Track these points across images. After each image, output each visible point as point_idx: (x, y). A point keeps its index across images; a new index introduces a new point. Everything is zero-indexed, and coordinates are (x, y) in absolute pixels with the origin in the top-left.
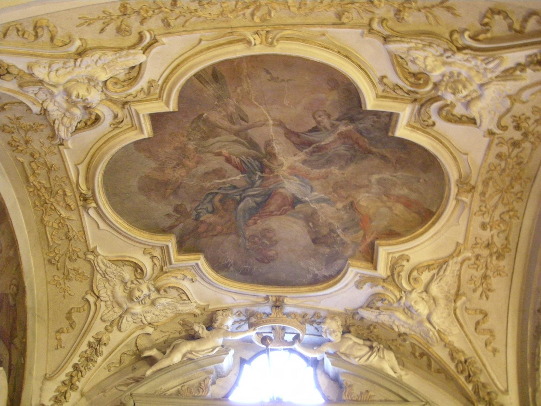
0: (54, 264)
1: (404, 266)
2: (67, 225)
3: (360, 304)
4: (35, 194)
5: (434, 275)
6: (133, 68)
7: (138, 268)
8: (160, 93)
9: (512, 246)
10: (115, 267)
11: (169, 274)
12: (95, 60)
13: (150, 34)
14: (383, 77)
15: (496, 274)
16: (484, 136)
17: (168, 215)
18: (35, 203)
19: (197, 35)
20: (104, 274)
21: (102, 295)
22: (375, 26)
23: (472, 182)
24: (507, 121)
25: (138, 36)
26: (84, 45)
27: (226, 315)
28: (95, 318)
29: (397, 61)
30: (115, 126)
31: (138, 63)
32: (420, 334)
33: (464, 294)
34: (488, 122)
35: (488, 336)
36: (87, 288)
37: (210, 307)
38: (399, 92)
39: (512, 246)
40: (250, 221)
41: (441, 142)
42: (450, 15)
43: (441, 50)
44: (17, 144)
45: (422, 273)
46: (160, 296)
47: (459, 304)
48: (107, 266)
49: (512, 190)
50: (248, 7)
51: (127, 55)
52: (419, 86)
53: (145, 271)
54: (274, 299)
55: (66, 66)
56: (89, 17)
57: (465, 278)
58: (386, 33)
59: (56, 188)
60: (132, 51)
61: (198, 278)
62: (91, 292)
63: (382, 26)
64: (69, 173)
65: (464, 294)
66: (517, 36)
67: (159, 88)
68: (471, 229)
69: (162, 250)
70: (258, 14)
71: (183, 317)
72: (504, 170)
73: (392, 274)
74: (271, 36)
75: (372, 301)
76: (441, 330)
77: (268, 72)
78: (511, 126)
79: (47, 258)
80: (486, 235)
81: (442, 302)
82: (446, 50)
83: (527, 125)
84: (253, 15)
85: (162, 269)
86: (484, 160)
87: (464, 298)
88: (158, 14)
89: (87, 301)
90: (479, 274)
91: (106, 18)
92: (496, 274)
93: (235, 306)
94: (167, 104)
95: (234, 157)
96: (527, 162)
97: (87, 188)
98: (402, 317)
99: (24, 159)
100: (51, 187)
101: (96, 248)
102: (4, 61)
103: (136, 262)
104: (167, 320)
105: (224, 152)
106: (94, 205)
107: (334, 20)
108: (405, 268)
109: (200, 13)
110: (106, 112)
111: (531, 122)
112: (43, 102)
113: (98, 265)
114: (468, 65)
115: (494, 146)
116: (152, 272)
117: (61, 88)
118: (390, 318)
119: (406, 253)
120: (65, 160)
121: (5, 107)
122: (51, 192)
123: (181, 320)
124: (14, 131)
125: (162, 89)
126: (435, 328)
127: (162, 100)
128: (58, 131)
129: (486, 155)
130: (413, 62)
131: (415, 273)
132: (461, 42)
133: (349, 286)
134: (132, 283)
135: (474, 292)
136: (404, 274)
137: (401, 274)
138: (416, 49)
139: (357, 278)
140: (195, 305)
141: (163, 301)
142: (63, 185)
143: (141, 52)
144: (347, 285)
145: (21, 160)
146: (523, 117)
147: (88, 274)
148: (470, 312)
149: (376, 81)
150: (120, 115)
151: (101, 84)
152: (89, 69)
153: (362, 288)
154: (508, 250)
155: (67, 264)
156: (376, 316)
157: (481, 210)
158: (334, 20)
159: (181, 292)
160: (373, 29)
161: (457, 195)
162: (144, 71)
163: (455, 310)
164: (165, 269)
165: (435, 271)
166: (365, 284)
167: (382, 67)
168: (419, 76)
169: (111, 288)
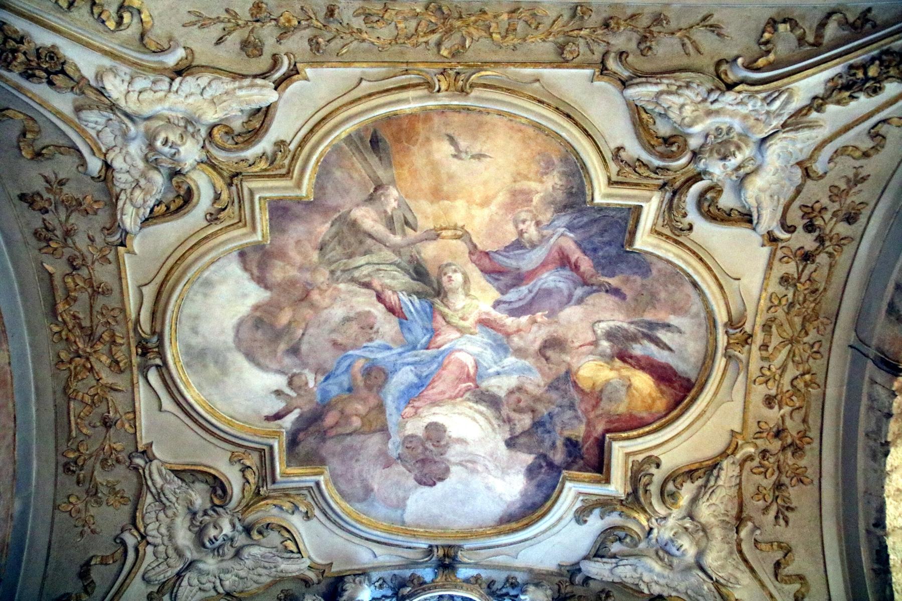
0: (74, 472)
1: (653, 475)
2: (107, 399)
3: (583, 552)
4: (62, 339)
5: (700, 487)
6: (259, 110)
7: (218, 487)
8: (290, 165)
9: (814, 433)
10: (180, 482)
11: (269, 501)
12: (202, 87)
13: (289, 59)
14: (619, 149)
15: (795, 479)
16: (763, 245)
17: (278, 393)
18: (59, 356)
19: (356, 71)
20: (159, 497)
21: (150, 533)
22: (612, 64)
23: (748, 328)
24: (795, 217)
25: (271, 61)
26: (189, 58)
27: (360, 582)
28: (132, 575)
29: (639, 118)
30: (214, 217)
31: (264, 105)
32: (686, 593)
33: (750, 519)
34: (768, 220)
35: (797, 586)
36: (125, 519)
37: (334, 569)
38: (641, 170)
39: (814, 433)
40: (407, 410)
41: (701, 259)
42: (714, 37)
43: (703, 90)
44: (50, 235)
45: (682, 485)
46: (249, 542)
47: (743, 534)
48: (166, 479)
49: (806, 339)
50: (433, 32)
51: (252, 86)
52: (672, 156)
53: (229, 491)
54: (441, 552)
55: (156, 88)
56: (205, 13)
57: (749, 490)
58: (625, 74)
59: (100, 330)
60: (259, 81)
61: (317, 512)
62: (131, 527)
63: (621, 61)
64: (126, 300)
65: (750, 519)
66: (812, 49)
67: (289, 157)
68: (751, 407)
69: (261, 457)
70: (447, 44)
71: (287, 586)
72: (791, 305)
73: (635, 491)
74: (462, 77)
75: (603, 543)
76: (722, 581)
77: (452, 140)
78: (800, 223)
79: (63, 460)
80: (773, 415)
81: (717, 533)
82: (710, 92)
83: (822, 223)
84: (439, 44)
85: (258, 493)
86: (763, 288)
87: (750, 524)
88: (305, 28)
89: (123, 543)
90: (768, 482)
91: (229, 21)
92: (795, 479)
93: (375, 568)
94: (299, 185)
95: (390, 293)
96: (825, 289)
97: (151, 329)
98: (657, 567)
99: (56, 267)
100: (92, 327)
101: (151, 444)
102: (62, 51)
103: (217, 475)
104: (259, 589)
105: (376, 283)
106: (158, 361)
107: (553, 57)
108: (655, 479)
109: (365, 36)
110: (204, 185)
111: (827, 216)
112: (108, 150)
113: (151, 477)
114: (743, 110)
115: (776, 263)
116: (240, 496)
117: (142, 127)
118: (635, 570)
119: (655, 453)
120: (123, 275)
121: (44, 151)
122: (91, 336)
123: (282, 591)
124: (50, 208)
125: (294, 158)
126: (712, 579)
127: (292, 178)
128: (122, 214)
129: (766, 278)
130: (664, 116)
131: (670, 487)
132: (732, 77)
133: (563, 523)
134: (205, 513)
135: (764, 514)
136: (654, 489)
137: (648, 488)
138: (670, 93)
139: (578, 504)
140: (308, 563)
141: (255, 550)
142: (113, 323)
143: (273, 85)
144: (561, 519)
145: (50, 269)
146: (817, 206)
147: (130, 493)
148: (763, 546)
149: (608, 156)
150: (225, 196)
151: (203, 132)
152: (191, 100)
153: (585, 522)
154: (807, 439)
155: (95, 473)
156: (611, 570)
157: (763, 375)
158: (553, 57)
159: (287, 535)
160: (607, 69)
161: (726, 348)
162: (269, 126)
163: (739, 545)
164: (263, 491)
165: (700, 482)
166: (591, 512)
167: (618, 131)
168: (673, 140)
169: (168, 520)
